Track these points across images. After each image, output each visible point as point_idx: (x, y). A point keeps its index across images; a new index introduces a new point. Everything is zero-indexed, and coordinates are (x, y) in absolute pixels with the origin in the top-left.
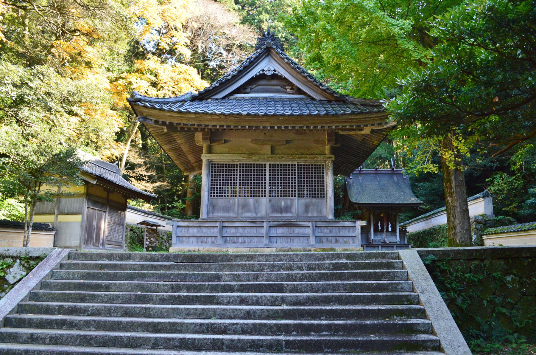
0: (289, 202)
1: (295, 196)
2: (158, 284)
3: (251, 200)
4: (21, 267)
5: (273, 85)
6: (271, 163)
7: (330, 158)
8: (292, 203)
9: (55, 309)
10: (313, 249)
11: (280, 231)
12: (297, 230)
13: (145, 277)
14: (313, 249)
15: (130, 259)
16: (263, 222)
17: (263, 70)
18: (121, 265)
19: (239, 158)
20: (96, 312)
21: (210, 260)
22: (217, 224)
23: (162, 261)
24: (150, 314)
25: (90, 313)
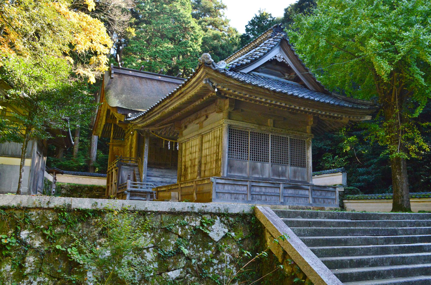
0: (284, 167)
1: (288, 164)
2: (377, 238)
3: (259, 164)
4: (222, 224)
5: (275, 70)
6: (273, 134)
7: (311, 136)
8: (286, 169)
9: (347, 263)
10: (312, 207)
11: (290, 191)
12: (301, 192)
13: (354, 233)
14: (312, 207)
15: (318, 217)
16: (280, 184)
17: (275, 57)
18: (324, 222)
19: (252, 127)
20: (375, 263)
21: (367, 218)
22: (248, 183)
23: (338, 219)
24: (405, 261)
25: (370, 264)
